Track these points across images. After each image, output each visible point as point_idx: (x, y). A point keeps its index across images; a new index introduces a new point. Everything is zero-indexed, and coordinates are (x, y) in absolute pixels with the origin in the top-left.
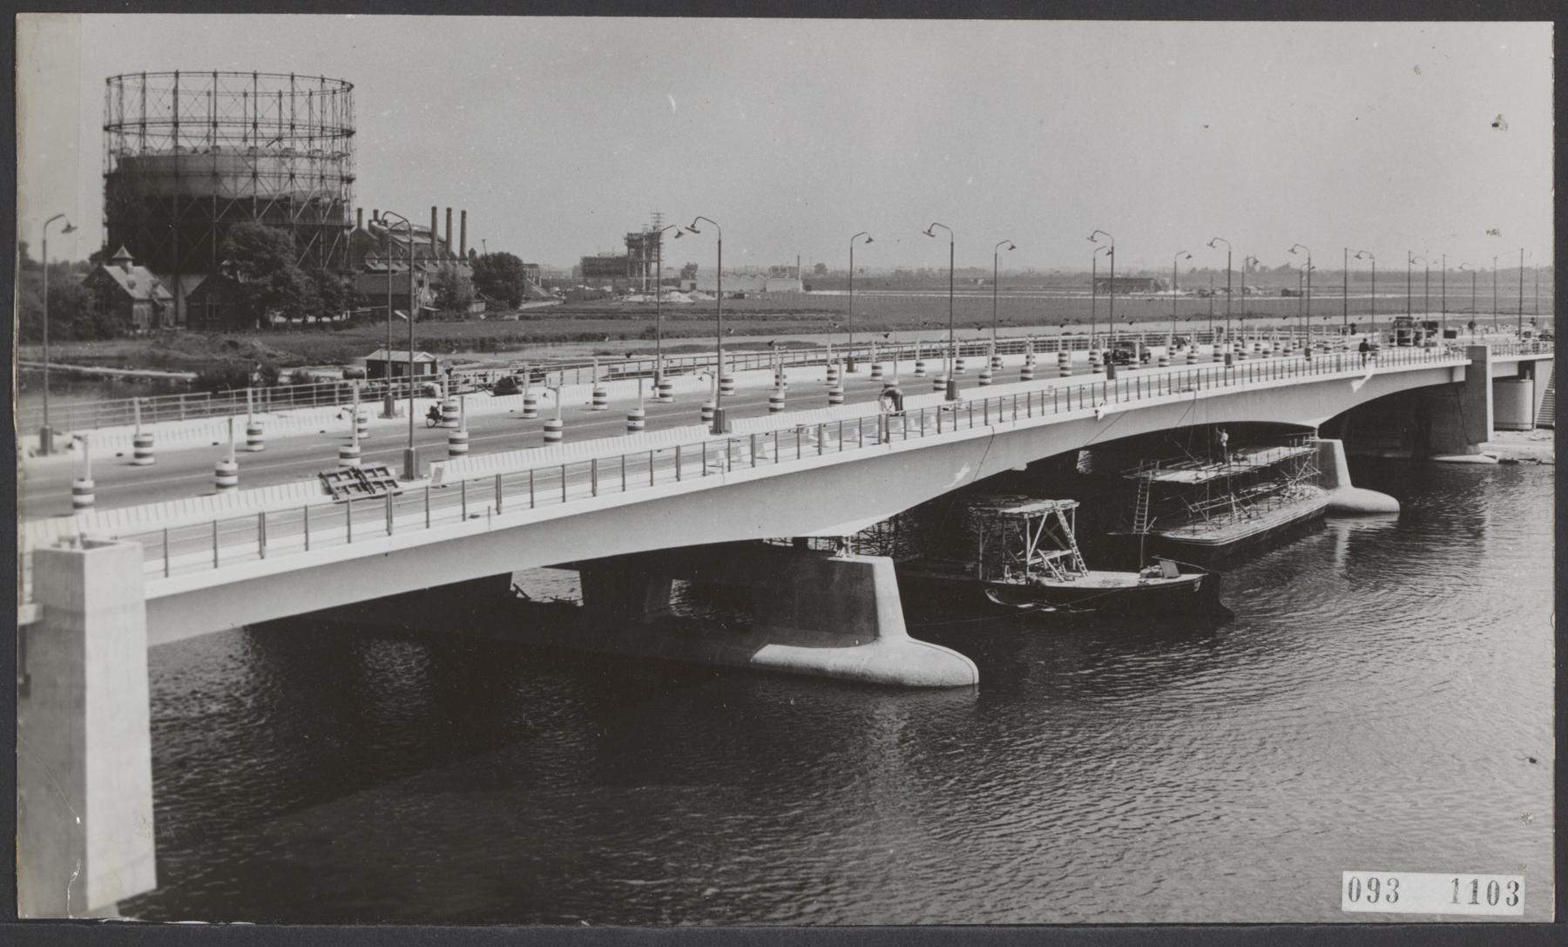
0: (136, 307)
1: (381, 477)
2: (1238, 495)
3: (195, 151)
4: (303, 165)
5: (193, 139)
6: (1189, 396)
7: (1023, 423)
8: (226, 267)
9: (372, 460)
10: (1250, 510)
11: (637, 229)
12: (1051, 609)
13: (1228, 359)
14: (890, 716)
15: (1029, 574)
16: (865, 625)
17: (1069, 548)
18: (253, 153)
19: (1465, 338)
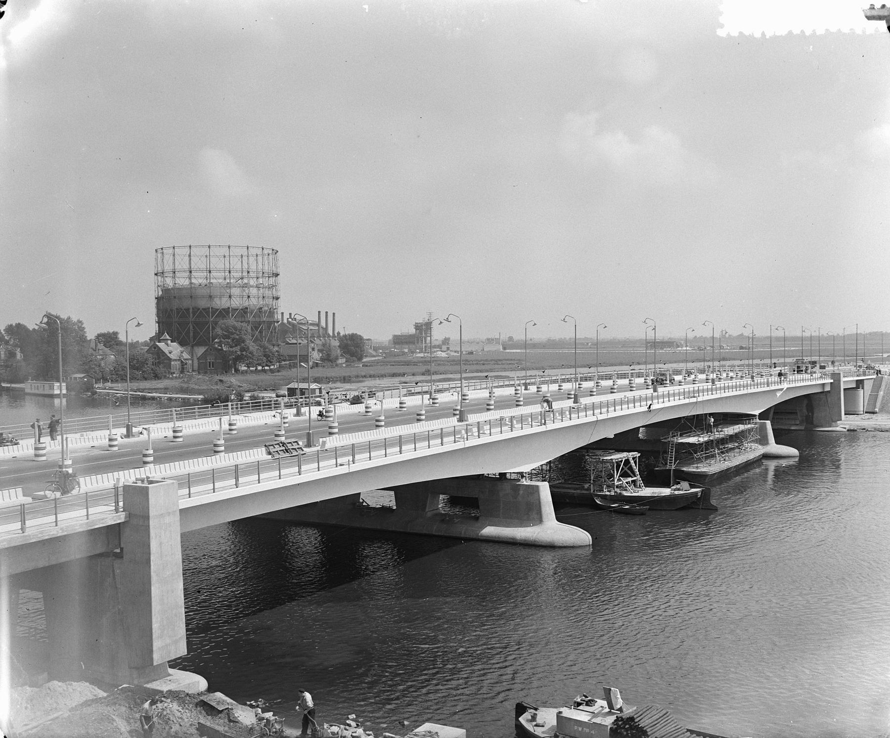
0: (172, 363)
2: (719, 449)
4: (254, 291)
5: (199, 279)
6: (694, 400)
7: (612, 414)
10: (725, 456)
13: (713, 381)
15: (616, 489)
18: (229, 286)
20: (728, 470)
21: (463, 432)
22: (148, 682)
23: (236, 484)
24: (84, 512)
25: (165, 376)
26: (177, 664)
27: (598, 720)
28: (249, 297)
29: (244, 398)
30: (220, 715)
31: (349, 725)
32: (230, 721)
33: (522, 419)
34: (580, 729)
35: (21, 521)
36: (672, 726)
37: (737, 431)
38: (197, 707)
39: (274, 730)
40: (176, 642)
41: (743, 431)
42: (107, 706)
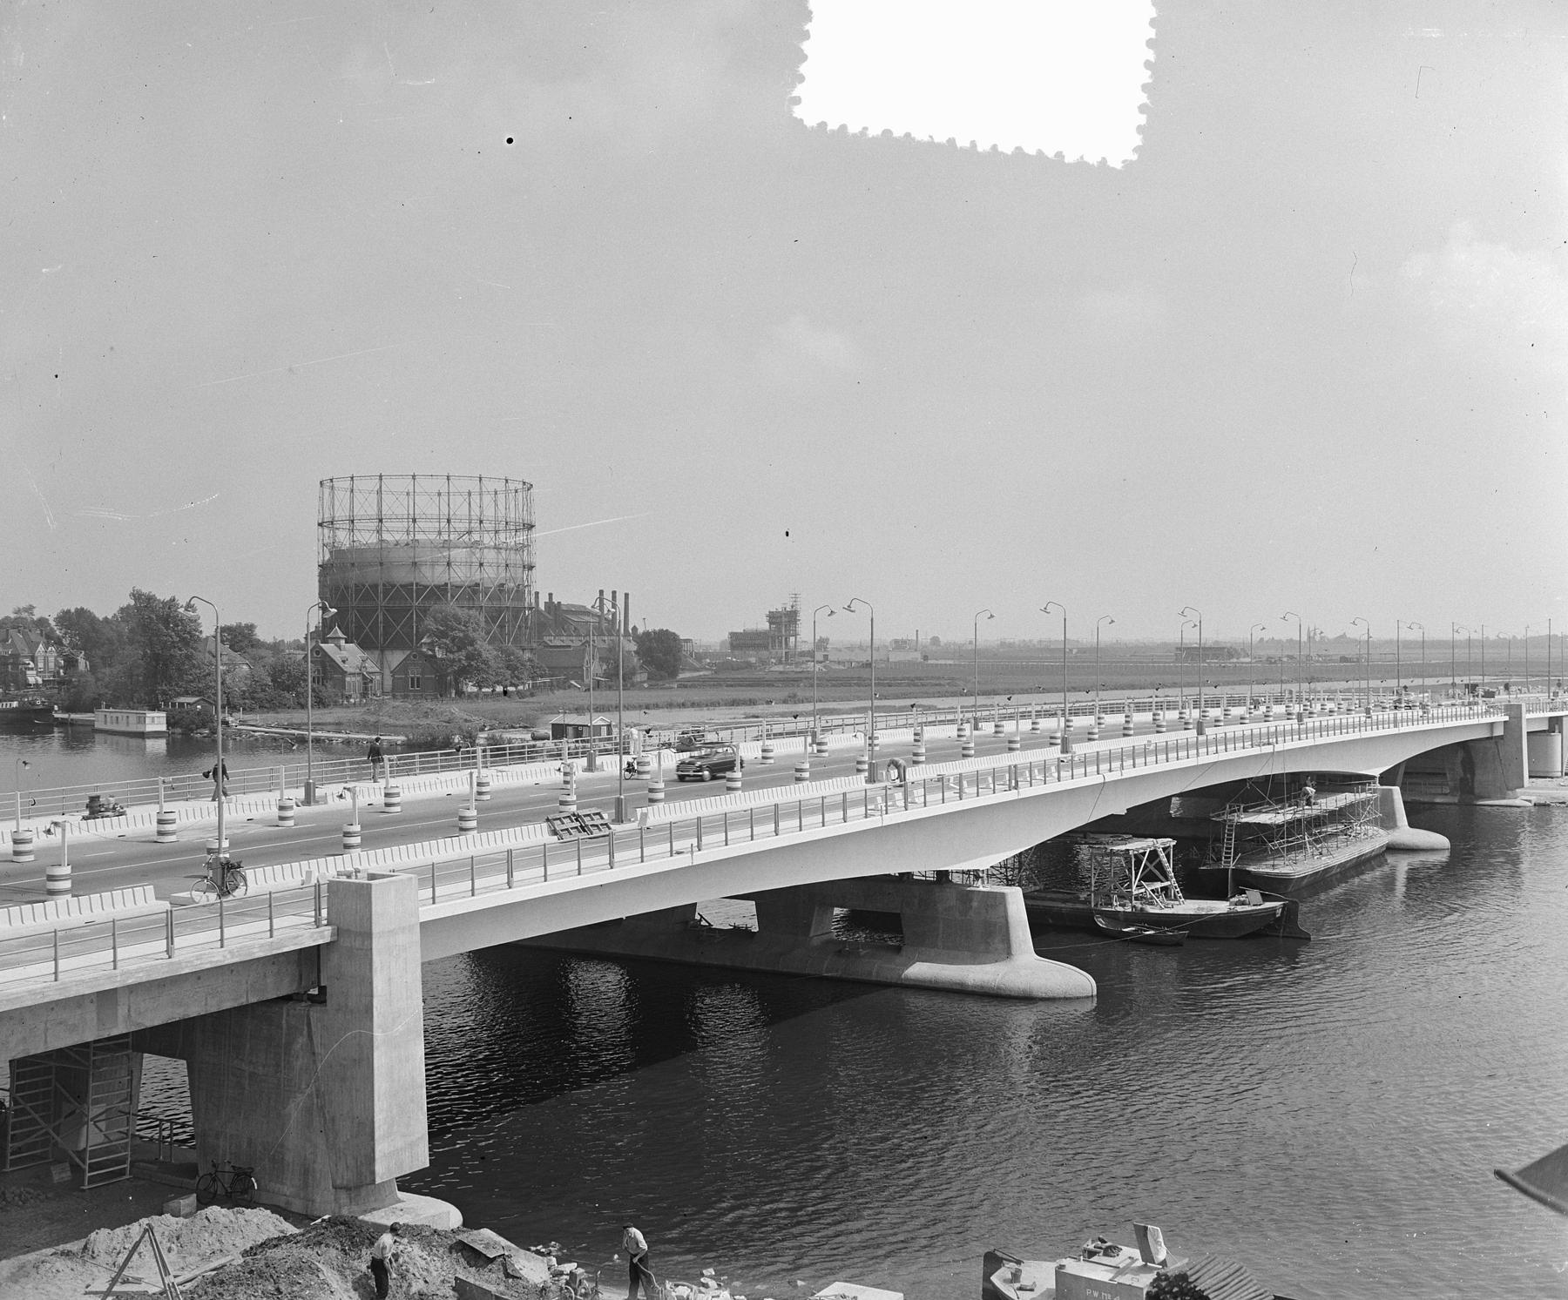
0: (348, 679)
1: (598, 821)
2: (1311, 835)
3: (397, 544)
4: (490, 555)
5: (395, 533)
6: (1268, 749)
7: (1130, 773)
8: (425, 644)
9: (589, 806)
10: (1322, 848)
11: (778, 607)
12: (1152, 932)
13: (1300, 718)
14: (1022, 1024)
15: (1134, 902)
16: (1000, 946)
17: (1167, 880)
18: (447, 545)
19: (1502, 697)
20: (1326, 871)
21: (879, 799)
22: (365, 1212)
23: (508, 883)
24: (108, 955)
25: (336, 702)
26: (410, 1183)
27: (1126, 1279)
28: (481, 565)
29: (477, 741)
30: (490, 1266)
31: (706, 1286)
32: (508, 1275)
33: (977, 779)
34: (1096, 1294)
35: (167, 938)
36: (1250, 1290)
37: (1341, 804)
38: (451, 1253)
39: (583, 1291)
40: (412, 1145)
41: (1352, 805)
42: (306, 1247)
